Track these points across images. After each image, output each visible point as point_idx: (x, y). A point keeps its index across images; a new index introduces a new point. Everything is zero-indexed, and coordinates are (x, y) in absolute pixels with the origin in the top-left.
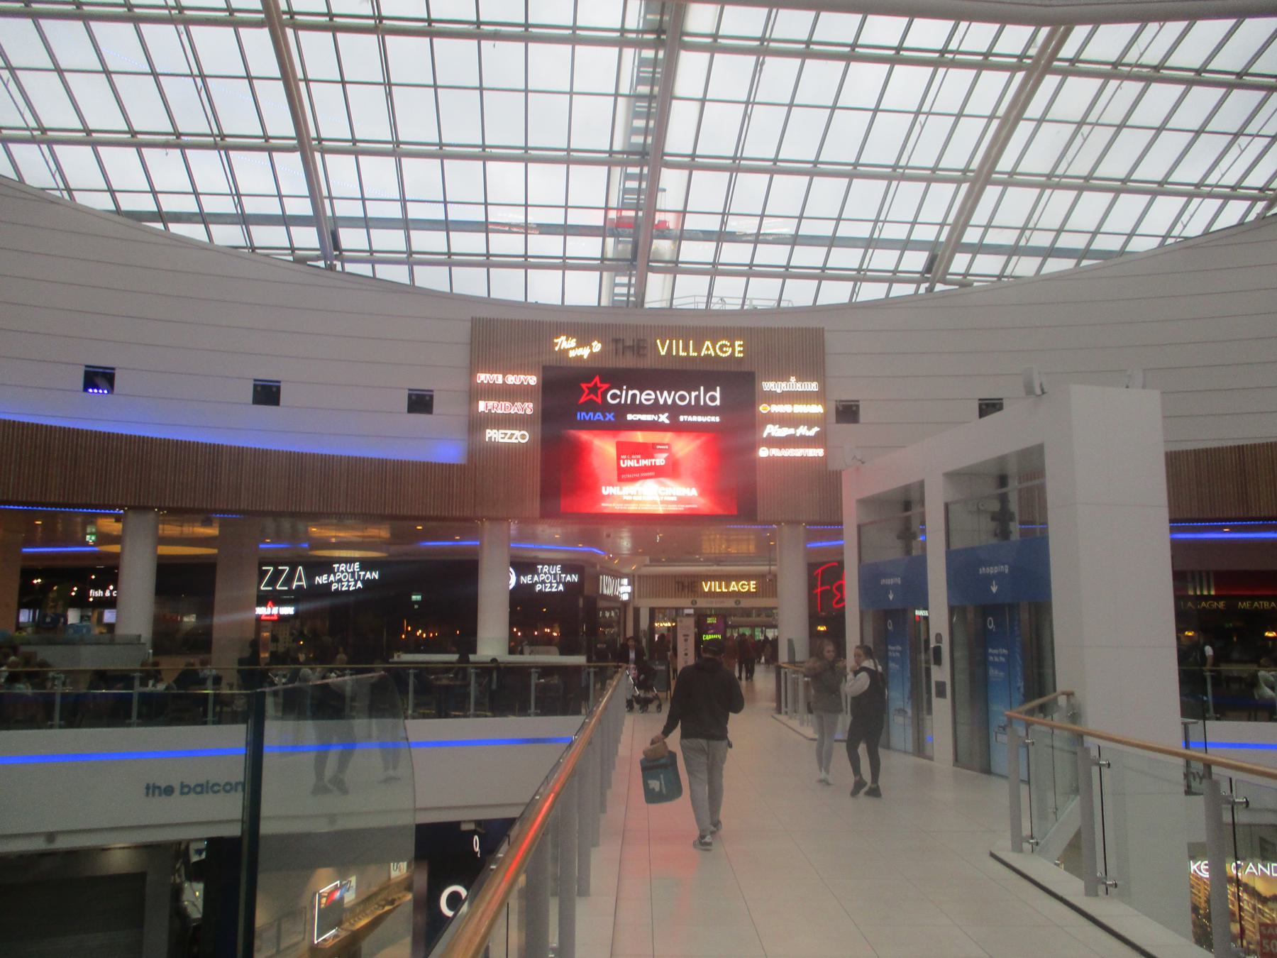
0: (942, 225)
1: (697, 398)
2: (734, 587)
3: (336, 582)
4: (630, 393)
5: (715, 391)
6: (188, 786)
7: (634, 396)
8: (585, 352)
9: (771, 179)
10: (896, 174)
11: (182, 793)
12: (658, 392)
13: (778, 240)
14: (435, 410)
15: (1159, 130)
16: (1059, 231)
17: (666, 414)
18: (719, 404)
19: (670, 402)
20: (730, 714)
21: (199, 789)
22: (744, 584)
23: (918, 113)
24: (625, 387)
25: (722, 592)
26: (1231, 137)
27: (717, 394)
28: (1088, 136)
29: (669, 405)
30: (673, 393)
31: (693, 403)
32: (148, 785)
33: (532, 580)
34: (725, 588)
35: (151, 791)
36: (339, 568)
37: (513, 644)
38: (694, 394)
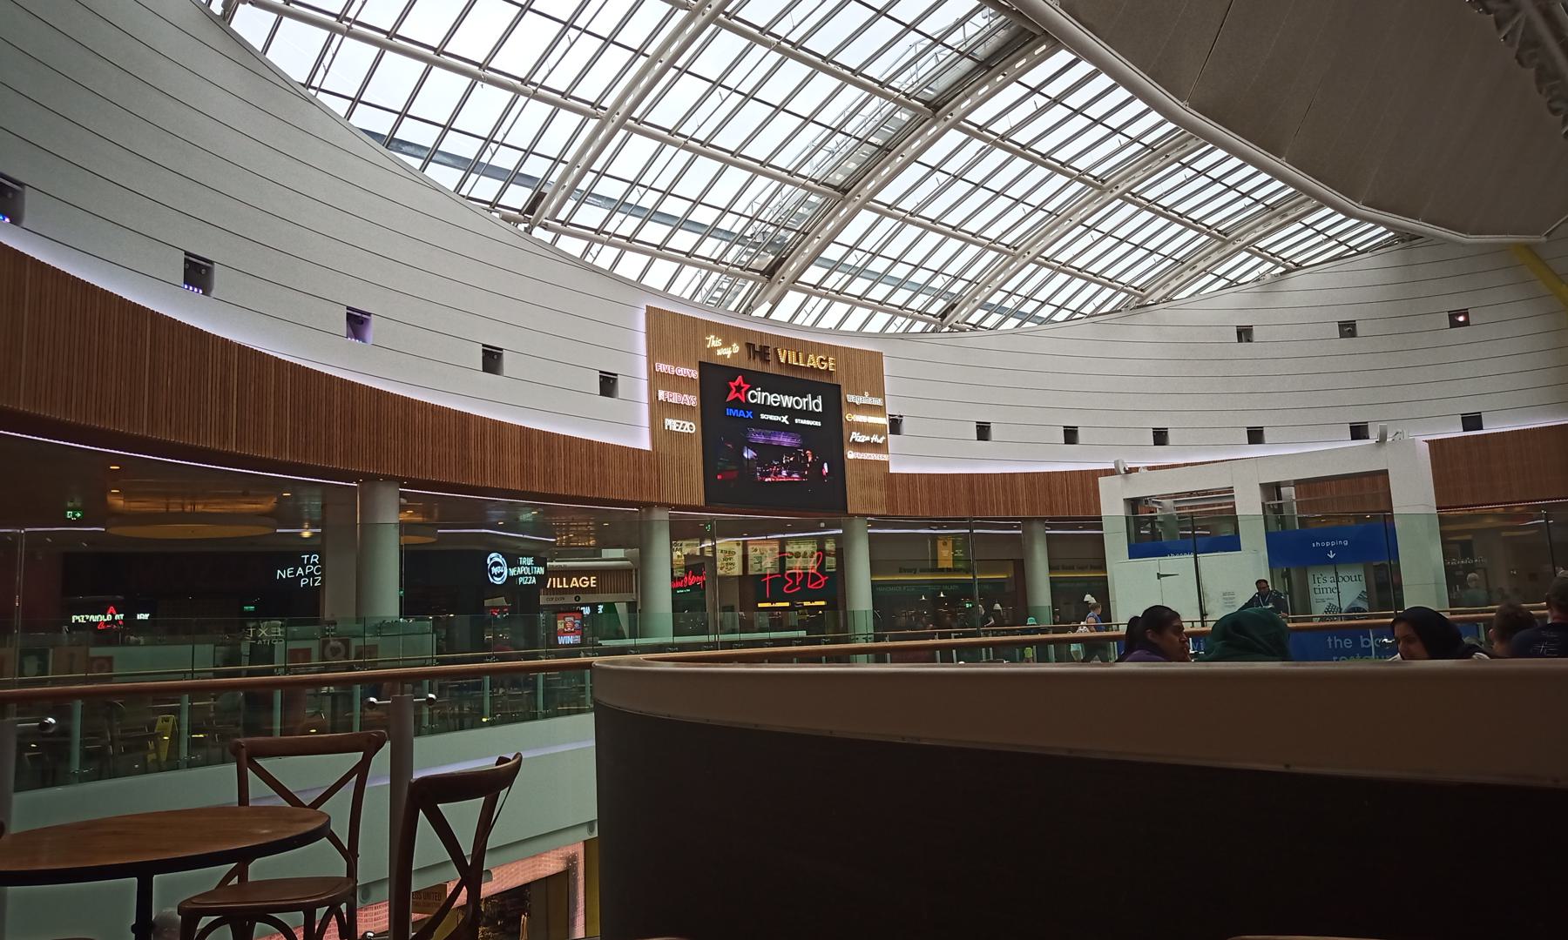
0: (557, 161)
8: (727, 352)
9: (528, 100)
10: (524, 88)
13: (455, 161)
15: (778, 109)
16: (696, 203)
17: (787, 417)
22: (584, 580)
23: (568, 25)
25: (563, 588)
26: (1148, 252)
28: (574, 42)
33: (295, 573)
34: (567, 584)
36: (309, 559)
38: (805, 400)
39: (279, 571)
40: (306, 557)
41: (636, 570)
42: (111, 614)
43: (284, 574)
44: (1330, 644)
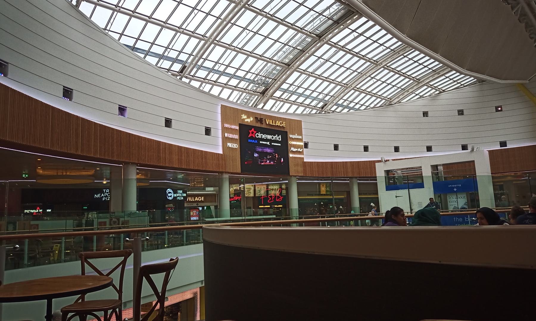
0: (190, 55)
2: (197, 199)
8: (249, 120)
9: (181, 34)
10: (179, 30)
13: (156, 55)
15: (266, 37)
16: (238, 69)
17: (269, 142)
22: (200, 198)
23: (194, 8)
25: (192, 201)
26: (392, 86)
28: (196, 14)
33: (101, 196)
34: (194, 199)
36: (106, 191)
38: (275, 137)
39: (95, 195)
40: (105, 190)
41: (217, 195)
42: (38, 210)
43: (97, 196)
44: (455, 220)
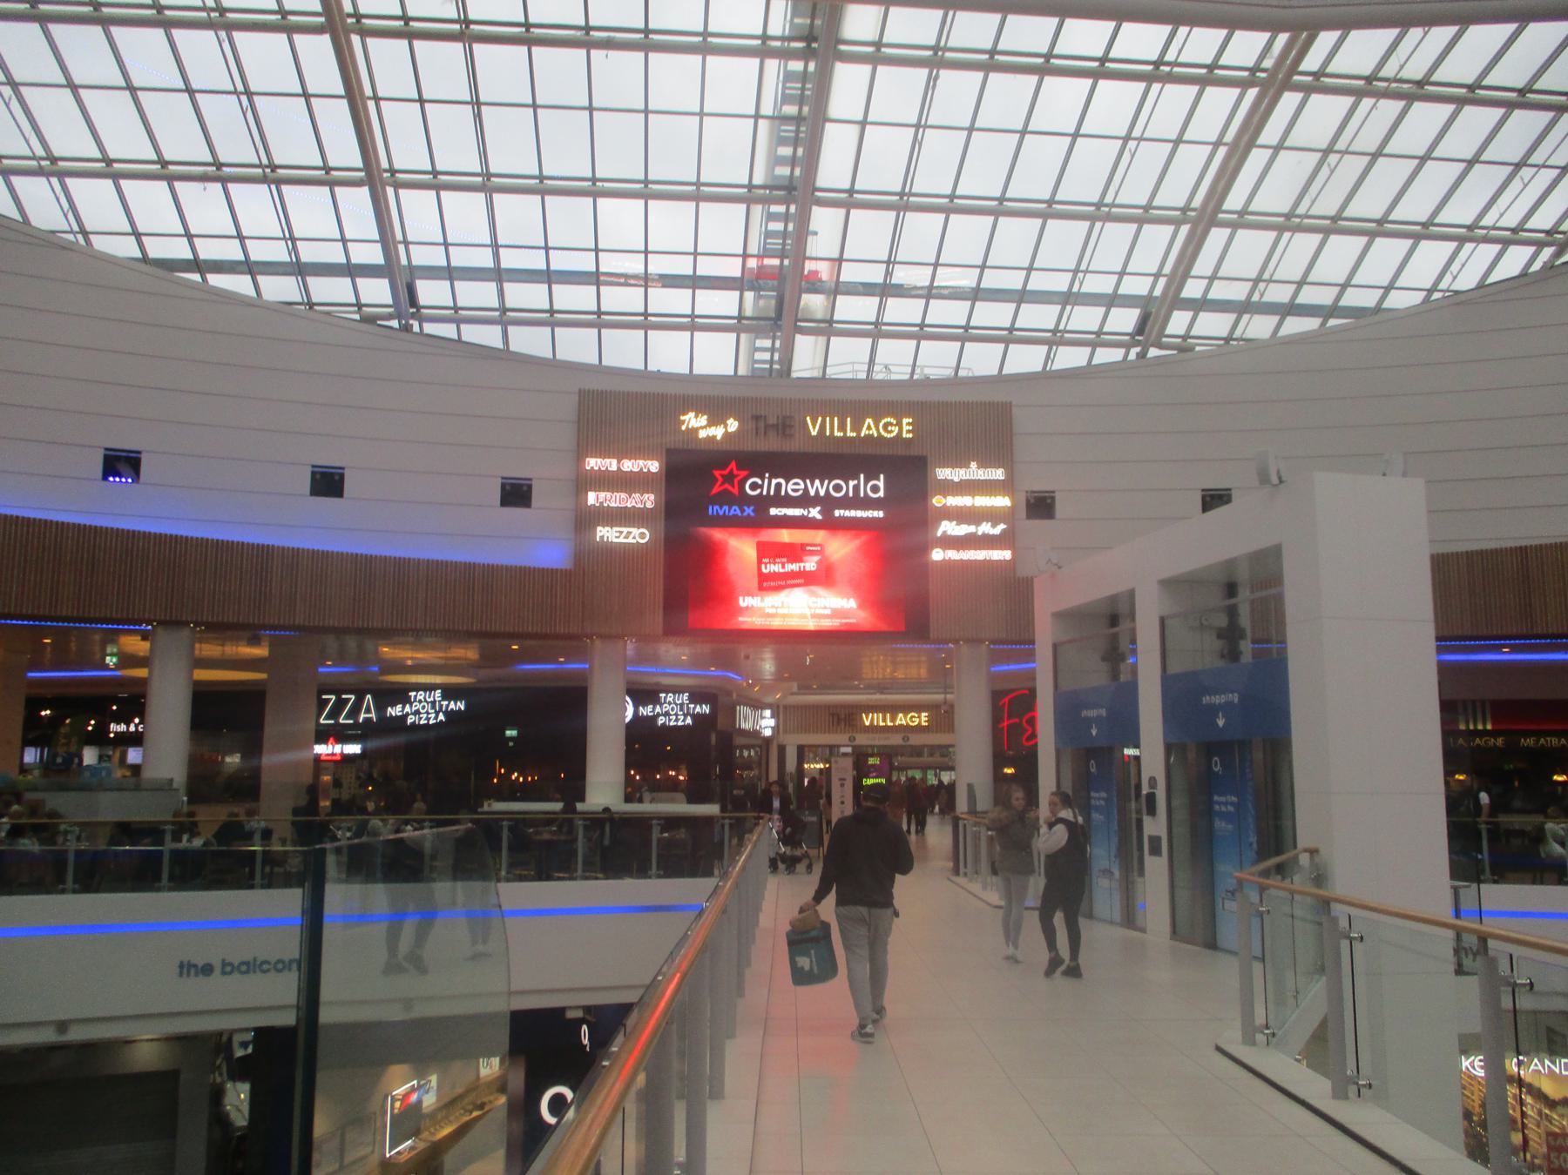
0: (1157, 276)
1: (856, 488)
3: (412, 714)
4: (774, 482)
5: (878, 479)
6: (231, 964)
7: (778, 486)
8: (718, 432)
9: (947, 220)
10: (1100, 213)
11: (224, 973)
12: (808, 481)
13: (955, 294)
14: (534, 502)
15: (1424, 159)
16: (1301, 284)
17: (818, 508)
18: (882, 496)
19: (822, 493)
20: (897, 875)
21: (244, 968)
22: (914, 717)
23: (1127, 138)
24: (767, 475)
25: (886, 726)
26: (1511, 168)
27: (881, 484)
28: (1336, 166)
29: (821, 497)
30: (826, 482)
31: (851, 494)
32: (182, 963)
33: (653, 711)
34: (891, 721)
35: (185, 970)
36: (416, 696)
37: (629, 790)
38: (852, 483)
